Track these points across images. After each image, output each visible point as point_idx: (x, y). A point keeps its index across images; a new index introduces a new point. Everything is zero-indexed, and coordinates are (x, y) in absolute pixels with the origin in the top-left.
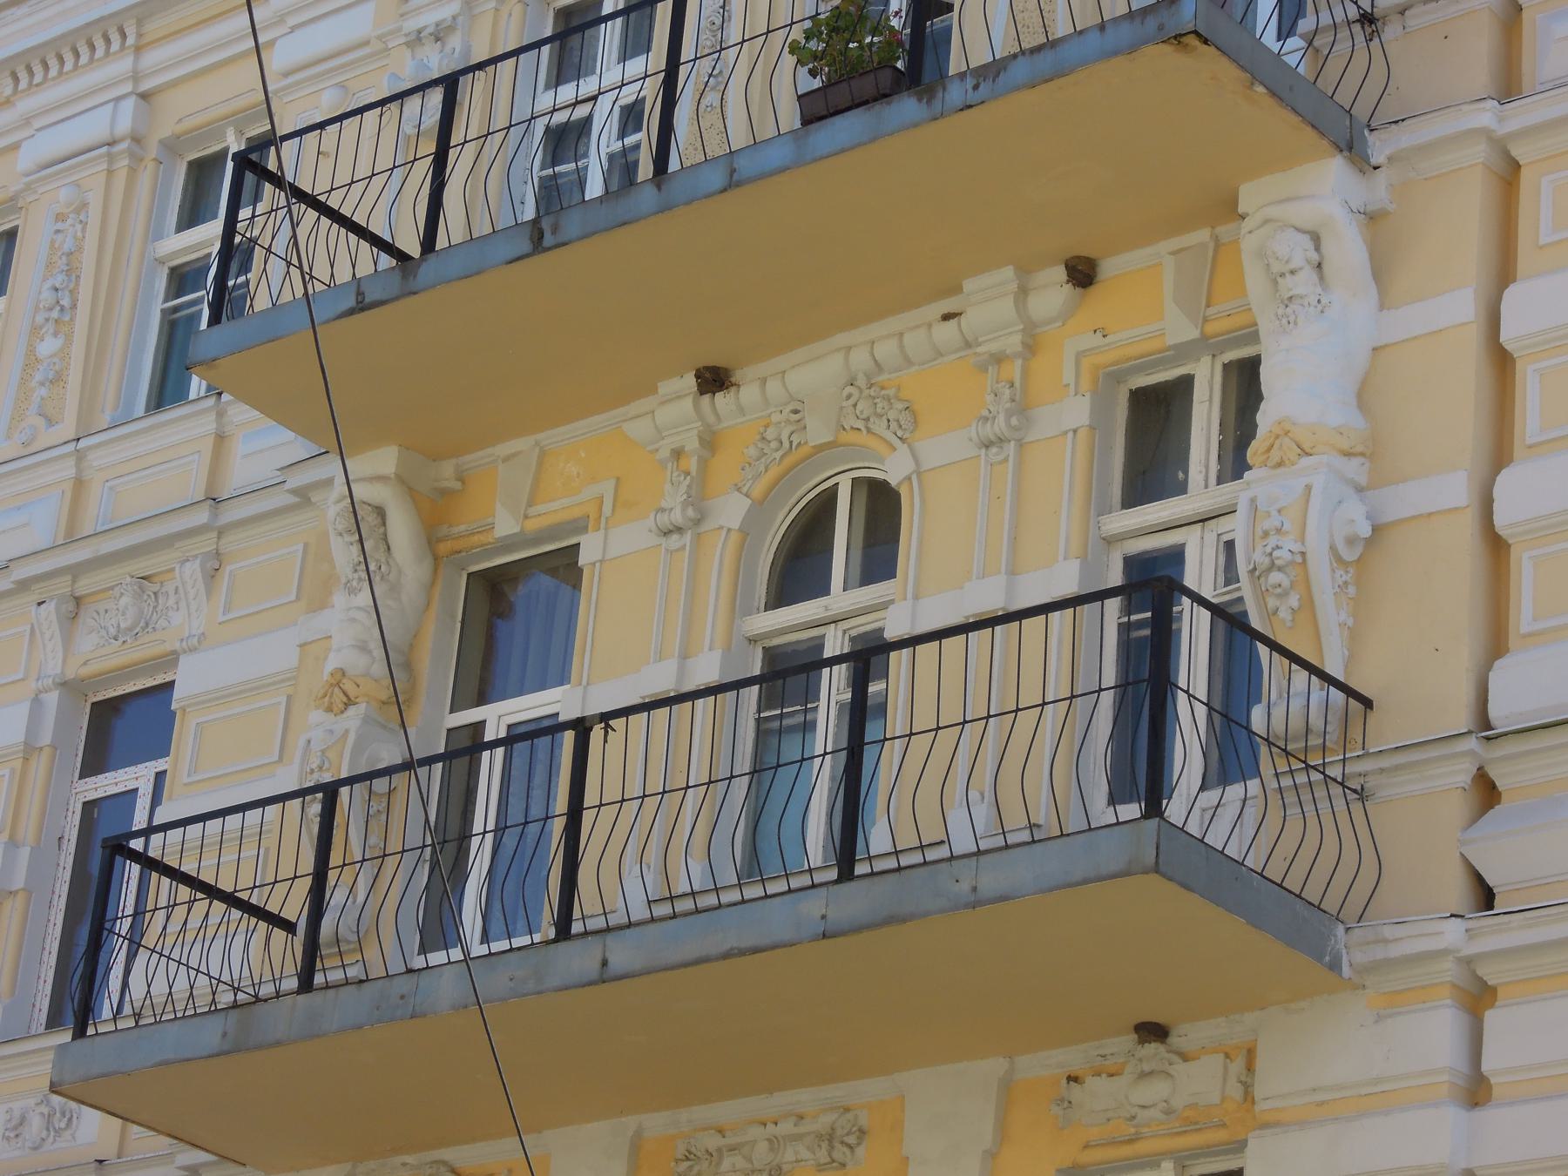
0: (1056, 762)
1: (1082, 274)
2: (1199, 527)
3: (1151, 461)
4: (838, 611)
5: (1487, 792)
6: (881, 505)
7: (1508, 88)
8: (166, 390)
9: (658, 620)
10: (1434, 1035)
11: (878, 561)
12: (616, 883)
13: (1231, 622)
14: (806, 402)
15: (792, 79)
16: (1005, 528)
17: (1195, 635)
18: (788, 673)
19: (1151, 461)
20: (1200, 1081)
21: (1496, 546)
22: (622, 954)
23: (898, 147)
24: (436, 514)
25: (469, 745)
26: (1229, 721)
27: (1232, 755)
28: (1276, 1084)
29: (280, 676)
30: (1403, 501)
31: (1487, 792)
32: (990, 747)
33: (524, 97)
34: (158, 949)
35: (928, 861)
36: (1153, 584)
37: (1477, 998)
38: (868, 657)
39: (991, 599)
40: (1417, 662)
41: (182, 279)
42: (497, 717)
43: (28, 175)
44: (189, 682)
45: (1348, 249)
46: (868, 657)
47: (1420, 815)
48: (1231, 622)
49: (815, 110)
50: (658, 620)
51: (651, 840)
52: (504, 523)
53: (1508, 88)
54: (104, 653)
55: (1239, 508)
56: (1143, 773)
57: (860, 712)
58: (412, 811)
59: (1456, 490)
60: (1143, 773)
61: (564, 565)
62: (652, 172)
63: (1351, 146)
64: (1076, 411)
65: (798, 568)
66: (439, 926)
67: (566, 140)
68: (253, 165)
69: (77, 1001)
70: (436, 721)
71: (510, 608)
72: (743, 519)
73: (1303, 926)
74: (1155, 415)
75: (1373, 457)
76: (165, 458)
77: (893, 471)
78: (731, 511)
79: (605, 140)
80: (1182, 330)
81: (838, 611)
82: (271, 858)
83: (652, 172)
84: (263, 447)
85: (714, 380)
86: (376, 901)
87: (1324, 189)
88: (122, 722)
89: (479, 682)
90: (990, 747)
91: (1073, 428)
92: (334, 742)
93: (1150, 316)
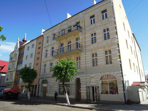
0: (75, 47)
1: (75, 36)
2: (78, 41)
3: (77, 40)
4: (70, 44)
5: (85, 47)
6: (71, 41)
7: (85, 30)
8: (53, 40)
9: (65, 45)
10: (84, 53)
11: (71, 43)
12: (65, 51)
13: (79, 44)
14: (68, 39)
15: (68, 31)
16: (73, 42)
17: (78, 44)
18: (69, 46)
19: (77, 40)
20: (79, 55)
21: (85, 42)
22: (65, 53)
23: (71, 33)
24: (60, 42)
25: (61, 48)
26: (79, 46)
27: (79, 47)
28: (81, 55)
29: (56, 47)
30: (83, 40)
31: (85, 47)
32: (74, 47)
33: (61, 32)
34: (85, 61)
35: (72, 50)
36: (77, 43)
37: (85, 52)
38: (70, 45)
39: (73, 44)
40: (83, 44)
41: (53, 37)
42: (62, 47)
43: (11, 44)
44: (54, 47)
45: (81, 34)
46: (70, 45)
47: (84, 48)
48: (79, 44)
49: (68, 32)
50: (65, 45)
51: (66, 50)
52: (62, 43)
53: (85, 30)
54: (52, 47)
55: (38, 44)
56: (77, 48)
57: (70, 47)
58: (60, 49)
59: (84, 40)
60: (77, 48)
61: (63, 43)
62: (64, 34)
63: (81, 32)
64: (75, 39)
65: (69, 43)
66: (61, 53)
67: (62, 33)
68: (55, 34)
69: (52, 55)
70: (60, 48)
71: (62, 45)
72: (67, 42)
73: (81, 51)
74: (77, 39)
75: (82, 39)
76: (53, 42)
77: (71, 41)
78: (67, 42)
79: (63, 33)
80: (77, 37)
81: (70, 44)
82: (56, 51)
83: (64, 34)
84: (56, 41)
85: (66, 39)
86: (59, 52)
87: (81, 33)
88: (53, 48)
89: (61, 46)
90: (74, 47)
91: (75, 39)
92: (58, 48)
93: (77, 37)
